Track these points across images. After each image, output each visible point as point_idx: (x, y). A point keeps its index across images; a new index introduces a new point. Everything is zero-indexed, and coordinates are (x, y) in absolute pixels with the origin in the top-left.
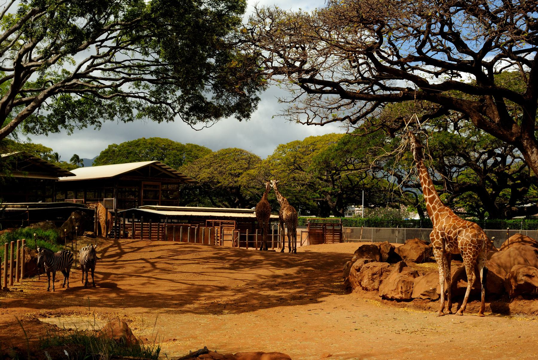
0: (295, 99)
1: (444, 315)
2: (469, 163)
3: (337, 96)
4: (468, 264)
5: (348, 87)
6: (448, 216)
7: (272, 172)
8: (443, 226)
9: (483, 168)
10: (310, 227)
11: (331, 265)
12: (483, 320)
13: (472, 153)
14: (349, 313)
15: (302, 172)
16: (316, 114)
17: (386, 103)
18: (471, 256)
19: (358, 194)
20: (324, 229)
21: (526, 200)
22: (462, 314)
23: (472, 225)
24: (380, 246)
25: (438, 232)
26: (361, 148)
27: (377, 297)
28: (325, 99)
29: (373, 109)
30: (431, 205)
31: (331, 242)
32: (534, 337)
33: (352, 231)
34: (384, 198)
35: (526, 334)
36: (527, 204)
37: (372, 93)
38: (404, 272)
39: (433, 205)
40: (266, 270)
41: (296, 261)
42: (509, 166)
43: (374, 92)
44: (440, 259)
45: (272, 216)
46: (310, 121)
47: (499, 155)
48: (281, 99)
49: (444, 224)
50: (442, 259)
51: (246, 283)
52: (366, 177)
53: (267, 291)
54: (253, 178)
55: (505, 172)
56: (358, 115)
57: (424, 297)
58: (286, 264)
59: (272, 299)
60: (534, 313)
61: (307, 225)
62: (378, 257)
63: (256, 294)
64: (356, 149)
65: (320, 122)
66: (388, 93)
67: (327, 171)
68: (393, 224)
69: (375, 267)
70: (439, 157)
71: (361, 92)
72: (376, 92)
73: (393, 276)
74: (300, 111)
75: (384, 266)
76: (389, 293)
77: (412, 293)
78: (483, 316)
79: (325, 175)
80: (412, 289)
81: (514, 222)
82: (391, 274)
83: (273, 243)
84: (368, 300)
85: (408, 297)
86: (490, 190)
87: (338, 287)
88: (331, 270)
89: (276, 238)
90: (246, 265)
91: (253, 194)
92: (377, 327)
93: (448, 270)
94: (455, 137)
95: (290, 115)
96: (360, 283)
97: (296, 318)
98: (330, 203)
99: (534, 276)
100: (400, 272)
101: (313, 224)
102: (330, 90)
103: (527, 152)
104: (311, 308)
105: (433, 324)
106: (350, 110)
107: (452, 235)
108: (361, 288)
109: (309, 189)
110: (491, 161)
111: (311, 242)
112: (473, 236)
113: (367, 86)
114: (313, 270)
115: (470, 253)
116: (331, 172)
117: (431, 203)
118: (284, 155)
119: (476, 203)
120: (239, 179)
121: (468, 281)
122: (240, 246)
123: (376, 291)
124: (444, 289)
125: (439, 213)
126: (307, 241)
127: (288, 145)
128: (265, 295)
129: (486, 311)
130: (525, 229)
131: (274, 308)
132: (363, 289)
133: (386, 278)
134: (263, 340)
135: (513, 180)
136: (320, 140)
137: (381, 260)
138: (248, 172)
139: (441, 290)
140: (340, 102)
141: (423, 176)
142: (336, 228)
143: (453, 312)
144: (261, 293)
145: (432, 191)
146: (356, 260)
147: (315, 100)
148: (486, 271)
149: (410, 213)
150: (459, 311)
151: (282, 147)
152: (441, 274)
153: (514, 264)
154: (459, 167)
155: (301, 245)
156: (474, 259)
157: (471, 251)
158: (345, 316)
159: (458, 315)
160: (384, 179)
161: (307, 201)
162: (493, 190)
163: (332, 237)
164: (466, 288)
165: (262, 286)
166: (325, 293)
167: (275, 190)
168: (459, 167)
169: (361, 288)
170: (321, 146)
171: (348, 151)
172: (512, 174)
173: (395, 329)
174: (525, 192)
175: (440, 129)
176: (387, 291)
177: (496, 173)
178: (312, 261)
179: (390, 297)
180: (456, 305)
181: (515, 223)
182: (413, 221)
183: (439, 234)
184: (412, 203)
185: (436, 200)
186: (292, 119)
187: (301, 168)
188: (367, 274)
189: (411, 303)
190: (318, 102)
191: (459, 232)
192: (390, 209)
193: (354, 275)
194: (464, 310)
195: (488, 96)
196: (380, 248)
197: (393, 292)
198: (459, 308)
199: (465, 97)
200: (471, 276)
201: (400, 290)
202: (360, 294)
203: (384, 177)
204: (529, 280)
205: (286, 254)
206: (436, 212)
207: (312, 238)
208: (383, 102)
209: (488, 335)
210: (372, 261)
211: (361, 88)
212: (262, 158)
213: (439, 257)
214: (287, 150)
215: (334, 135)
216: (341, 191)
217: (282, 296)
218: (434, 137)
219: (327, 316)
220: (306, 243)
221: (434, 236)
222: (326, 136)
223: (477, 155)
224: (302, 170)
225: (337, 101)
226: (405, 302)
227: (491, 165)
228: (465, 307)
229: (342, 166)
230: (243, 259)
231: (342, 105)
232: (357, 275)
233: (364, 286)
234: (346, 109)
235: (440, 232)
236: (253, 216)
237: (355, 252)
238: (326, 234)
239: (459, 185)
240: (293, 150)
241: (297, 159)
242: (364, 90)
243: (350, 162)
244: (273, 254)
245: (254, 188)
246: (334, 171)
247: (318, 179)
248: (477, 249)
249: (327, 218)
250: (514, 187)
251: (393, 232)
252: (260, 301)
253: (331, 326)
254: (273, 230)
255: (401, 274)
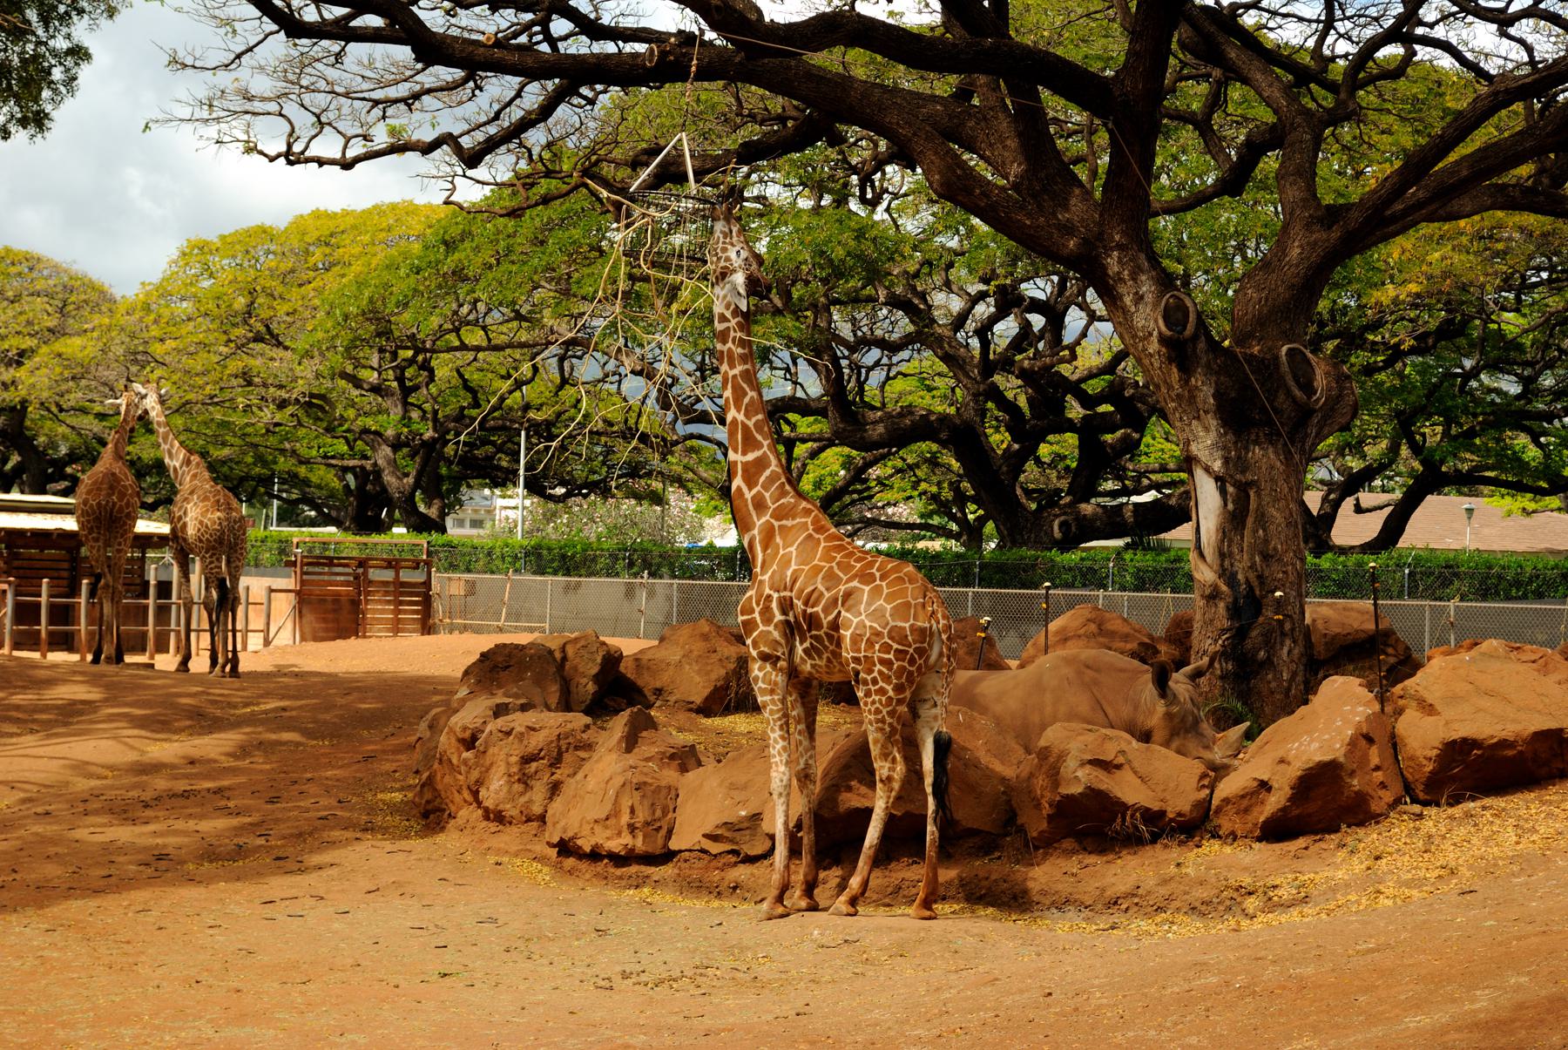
0: (239, 56)
1: (787, 915)
2: (924, 334)
3: (404, 53)
4: (878, 721)
5: (453, 21)
6: (810, 536)
7: (157, 349)
8: (789, 573)
9: (977, 353)
10: (303, 573)
11: (369, 721)
12: (928, 930)
13: (938, 298)
14: (425, 910)
15: (280, 353)
16: (323, 119)
17: (599, 87)
18: (889, 688)
19: (504, 443)
20: (361, 582)
21: (1138, 480)
22: (852, 910)
23: (895, 570)
24: (563, 649)
25: (769, 596)
26: (513, 262)
27: (540, 848)
28: (360, 63)
29: (546, 111)
30: (750, 489)
31: (388, 630)
32: (1098, 995)
33: (471, 588)
34: (604, 463)
35: (1072, 983)
36: (1140, 493)
37: (545, 48)
38: (645, 749)
39: (754, 491)
40: (110, 742)
41: (235, 707)
42: (1072, 348)
43: (552, 41)
44: (773, 701)
45: (143, 526)
46: (297, 148)
47: (1036, 306)
48: (181, 55)
49: (793, 567)
50: (783, 701)
51: (22, 795)
52: (532, 379)
53: (104, 825)
54: (79, 373)
55: (1058, 372)
56: (492, 130)
57: (715, 848)
58: (191, 718)
59: (121, 859)
60: (1116, 903)
61: (294, 564)
62: (554, 690)
63: (53, 841)
64: (491, 267)
65: (338, 156)
66: (610, 47)
67: (381, 350)
68: (631, 564)
69: (534, 729)
70: (814, 306)
71: (499, 44)
72: (561, 46)
73: (600, 766)
74: (258, 106)
75: (569, 726)
76: (586, 831)
77: (670, 832)
78: (930, 918)
79: (372, 368)
80: (670, 815)
81: (1082, 559)
82: (595, 756)
83: (151, 634)
84: (505, 859)
85: (656, 847)
86: (999, 440)
87: (393, 809)
88: (370, 743)
89: (163, 612)
90: (25, 721)
91: (80, 434)
92: (529, 965)
93: (806, 743)
94: (874, 233)
95: (218, 120)
96: (475, 794)
97: (211, 931)
98: (389, 478)
99: (1119, 767)
100: (629, 750)
101: (321, 560)
102: (377, 29)
103: (1121, 297)
104: (275, 894)
105: (743, 949)
106: (459, 111)
107: (818, 609)
108: (480, 812)
109: (305, 419)
110: (1006, 329)
111: (307, 630)
112: (896, 612)
113: (529, 16)
114: (298, 744)
115: (887, 679)
116: (395, 355)
117: (750, 483)
118: (206, 284)
119: (955, 487)
120: (21, 373)
121: (879, 785)
122: (17, 645)
123: (535, 824)
124: (787, 816)
125: (776, 524)
126: (289, 625)
127: (224, 243)
128: (93, 844)
129: (944, 899)
130: (1123, 589)
131: (124, 895)
132: (487, 818)
133: (575, 774)
134: (64, 1025)
135: (1087, 401)
136: (354, 227)
137: (566, 705)
138: (60, 346)
139: (777, 824)
140: (417, 78)
141: (734, 377)
142: (407, 576)
143: (822, 905)
144: (81, 834)
145: (759, 438)
146: (463, 701)
147: (318, 65)
148: (943, 747)
149: (708, 522)
150: (843, 898)
151: (201, 249)
152: (777, 759)
153: (1055, 720)
154: (892, 348)
155: (267, 643)
156: (900, 702)
157: (890, 669)
158: (409, 924)
159: (839, 914)
160: (607, 386)
161: (302, 471)
162: (1014, 440)
163: (392, 612)
164: (868, 812)
165: (85, 806)
166: (336, 834)
167: (159, 424)
168: (892, 348)
169: (480, 812)
170: (357, 250)
171: (459, 275)
172: (1084, 380)
173: (595, 970)
174: (1130, 447)
175: (821, 198)
176: (577, 825)
177: (1024, 374)
178: (300, 707)
179: (588, 849)
180: (832, 876)
181: (1088, 563)
182: (710, 551)
183: (774, 605)
184: (711, 485)
185: (767, 473)
186: (227, 139)
187: (275, 337)
188: (502, 756)
189: (667, 871)
190: (332, 74)
191: (848, 595)
192: (628, 505)
193: (455, 761)
194: (863, 893)
195: (982, 79)
196: (564, 659)
197: (598, 829)
198: (842, 887)
199: (904, 78)
200: (887, 765)
201: (625, 818)
202: (476, 838)
203: (603, 380)
204: (1104, 782)
205: (199, 679)
206: (763, 520)
207: (309, 617)
208: (591, 83)
209: (938, 989)
210: (524, 708)
211: (504, 25)
212: (117, 292)
213: (772, 692)
214: (219, 262)
215: (410, 209)
216: (435, 430)
217: (165, 846)
218: (797, 230)
219: (336, 925)
220: (285, 635)
221: (753, 611)
222: (378, 210)
223: (956, 304)
224: (279, 344)
225: (408, 73)
226: (643, 868)
227: (1008, 341)
228: (865, 884)
229: (441, 332)
230: (18, 699)
231: (429, 91)
232: (465, 762)
233: (489, 803)
234: (440, 105)
235: (776, 595)
236: (70, 524)
237: (466, 673)
238: (367, 602)
239: (889, 416)
240: (246, 264)
241: (260, 300)
242: (516, 35)
243: (471, 317)
244: (148, 678)
245: (84, 411)
246: (410, 353)
247: (342, 383)
248: (912, 662)
249: (376, 538)
250: (1089, 430)
251: (630, 592)
252: (74, 868)
253: (350, 961)
254: (153, 582)
255: (631, 759)
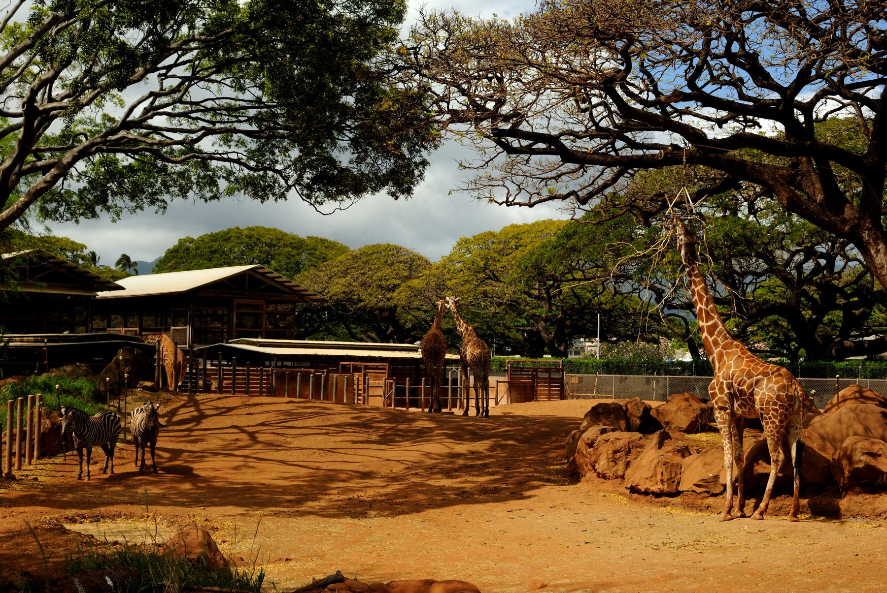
0: (487, 163)
1: (732, 519)
2: (773, 269)
3: (556, 159)
4: (771, 435)
5: (574, 144)
6: (739, 356)
7: (449, 283)
8: (731, 372)
9: (796, 276)
10: (511, 374)
11: (546, 436)
12: (796, 526)
13: (778, 253)
14: (576, 515)
15: (498, 284)
16: (521, 187)
17: (636, 169)
18: (777, 421)
19: (590, 319)
20: (535, 378)
21: (867, 330)
22: (761, 517)
23: (778, 370)
24: (626, 406)
25: (722, 382)
26: (595, 243)
27: (622, 489)
28: (536, 163)
29: (614, 180)
30: (711, 337)
31: (547, 398)
32: (880, 555)
33: (581, 380)
34: (633, 327)
35: (867, 550)
36: (868, 336)
37: (613, 153)
38: (666, 448)
39: (713, 338)
40: (439, 445)
41: (488, 430)
42: (840, 273)
43: (616, 151)
44: (725, 427)
45: (448, 356)
46: (511, 199)
47: (822, 256)
48: (464, 164)
49: (733, 369)
50: (729, 427)
51: (406, 466)
52: (603, 292)
53: (439, 479)
54: (417, 293)
55: (833, 284)
56: (591, 189)
57: (699, 490)
58: (471, 435)
59: (448, 492)
60: (880, 515)
61: (506, 371)
62: (623, 424)
63: (422, 485)
64: (586, 246)
65: (527, 202)
66: (640, 152)
67: (540, 282)
68: (647, 370)
69: (618, 439)
70: (724, 258)
71: (595, 152)
72: (620, 152)
73: (648, 454)
74: (494, 183)
75: (633, 438)
76: (642, 482)
77: (679, 483)
78: (796, 521)
79: (536, 289)
80: (679, 476)
81: (847, 365)
82: (645, 451)
83: (450, 400)
84: (607, 494)
85: (673, 489)
86: (807, 314)
87: (557, 472)
88: (545, 445)
89: (454, 391)
90: (405, 436)
91: (417, 319)
92: (622, 539)
93: (739, 445)
94: (750, 226)
95: (478, 189)
96: (594, 467)
97: (488, 523)
98: (544, 335)
99: (880, 455)
100: (660, 448)
101: (516, 369)
102: (544, 149)
103: (869, 251)
104: (513, 508)
105: (714, 534)
106: (577, 181)
107: (745, 387)
108: (596, 474)
109: (509, 311)
110: (809, 266)
111: (513, 398)
112: (779, 389)
113: (606, 141)
114: (515, 446)
115: (775, 417)
116: (545, 284)
117: (711, 334)
118: (468, 256)
119: (785, 334)
120: (394, 294)
121: (772, 463)
122: (396, 406)
123: (619, 479)
124: (732, 476)
125: (724, 351)
126: (506, 396)
127: (475, 239)
128: (436, 486)
129: (801, 513)
130: (866, 378)
131: (451, 507)
132: (598, 476)
133: (636, 458)
134: (433, 561)
135: (846, 296)
136: (528, 231)
137: (629, 428)
138: (409, 283)
139: (727, 479)
140: (560, 168)
141: (698, 291)
142: (555, 375)
143: (747, 515)
144: (431, 482)
145: (713, 315)
146: (587, 428)
147: (519, 165)
148: (801, 446)
149: (677, 351)
150: (757, 512)
151: (466, 242)
152: (727, 452)
153: (848, 436)
154: (758, 275)
155: (497, 403)
156: (781, 427)
157: (777, 413)
158: (570, 521)
159: (755, 519)
160: (634, 294)
161: (506, 332)
162: (814, 313)
163: (548, 390)
164: (768, 475)
165: (432, 470)
166: (535, 483)
167: (454, 313)
168: (758, 275)
169: (596, 474)
170: (529, 240)
171: (574, 249)
172: (844, 287)
173: (651, 542)
174: (866, 315)
175: (726, 212)
176: (638, 480)
177: (817, 285)
178: (515, 430)
179: (643, 490)
180: (751, 502)
181: (850, 367)
182: (681, 364)
183: (724, 386)
184: (679, 335)
185: (718, 329)
186: (482, 196)
187: (496, 277)
188: (605, 451)
189: (678, 500)
190: (525, 168)
191: (757, 382)
192: (642, 344)
193: (584, 453)
194: (766, 510)
195: (804, 159)
196: (627, 409)
197: (647, 481)
198: (756, 507)
199: (767, 160)
200: (776, 454)
201: (659, 477)
202: (594, 485)
203: (632, 292)
204: (872, 462)
205: (472, 418)
206: (718, 350)
207: (514, 393)
208: (632, 168)
209: (805, 552)
210: (613, 430)
211: (595, 145)
212: (432, 261)
213: (724, 423)
214: (474, 247)
215: (550, 223)
216: (562, 314)
217: (465, 487)
218: (716, 226)
219: (539, 521)
220: (504, 401)
221: (715, 389)
222: (537, 224)
223: (786, 256)
224: (498, 280)
225: (556, 167)
226: (667, 498)
227: (809, 272)
228: (767, 506)
229: (563, 274)
230: (401, 427)
231: (565, 174)
232: (589, 453)
233: (599, 471)
234: (570, 179)
235: (725, 382)
236: (418, 355)
237: (586, 415)
238: (538, 386)
239: (757, 304)
240: (484, 247)
241: (490, 262)
242: (601, 149)
243: (577, 267)
244: (451, 418)
245: (419, 309)
246: (551, 282)
247: (524, 296)
248: (787, 410)
249: (539, 360)
250: (847, 309)
251: (648, 382)
252: (429, 496)
253: (546, 536)
254: (450, 379)
255: (661, 452)
